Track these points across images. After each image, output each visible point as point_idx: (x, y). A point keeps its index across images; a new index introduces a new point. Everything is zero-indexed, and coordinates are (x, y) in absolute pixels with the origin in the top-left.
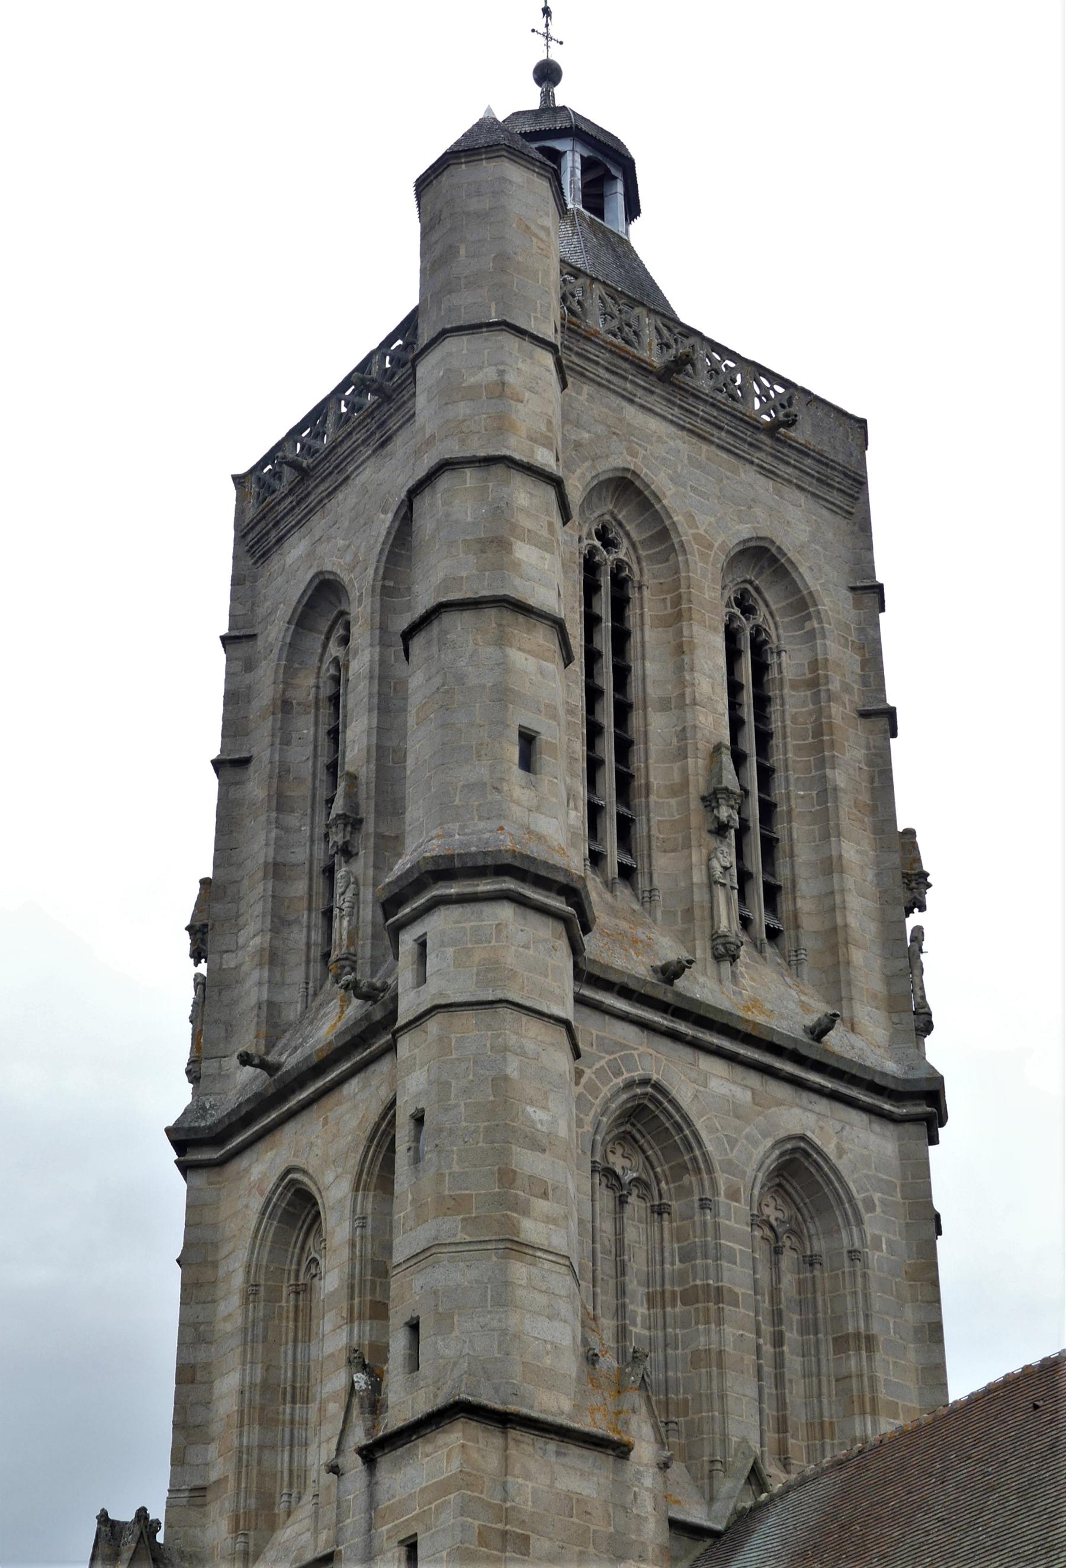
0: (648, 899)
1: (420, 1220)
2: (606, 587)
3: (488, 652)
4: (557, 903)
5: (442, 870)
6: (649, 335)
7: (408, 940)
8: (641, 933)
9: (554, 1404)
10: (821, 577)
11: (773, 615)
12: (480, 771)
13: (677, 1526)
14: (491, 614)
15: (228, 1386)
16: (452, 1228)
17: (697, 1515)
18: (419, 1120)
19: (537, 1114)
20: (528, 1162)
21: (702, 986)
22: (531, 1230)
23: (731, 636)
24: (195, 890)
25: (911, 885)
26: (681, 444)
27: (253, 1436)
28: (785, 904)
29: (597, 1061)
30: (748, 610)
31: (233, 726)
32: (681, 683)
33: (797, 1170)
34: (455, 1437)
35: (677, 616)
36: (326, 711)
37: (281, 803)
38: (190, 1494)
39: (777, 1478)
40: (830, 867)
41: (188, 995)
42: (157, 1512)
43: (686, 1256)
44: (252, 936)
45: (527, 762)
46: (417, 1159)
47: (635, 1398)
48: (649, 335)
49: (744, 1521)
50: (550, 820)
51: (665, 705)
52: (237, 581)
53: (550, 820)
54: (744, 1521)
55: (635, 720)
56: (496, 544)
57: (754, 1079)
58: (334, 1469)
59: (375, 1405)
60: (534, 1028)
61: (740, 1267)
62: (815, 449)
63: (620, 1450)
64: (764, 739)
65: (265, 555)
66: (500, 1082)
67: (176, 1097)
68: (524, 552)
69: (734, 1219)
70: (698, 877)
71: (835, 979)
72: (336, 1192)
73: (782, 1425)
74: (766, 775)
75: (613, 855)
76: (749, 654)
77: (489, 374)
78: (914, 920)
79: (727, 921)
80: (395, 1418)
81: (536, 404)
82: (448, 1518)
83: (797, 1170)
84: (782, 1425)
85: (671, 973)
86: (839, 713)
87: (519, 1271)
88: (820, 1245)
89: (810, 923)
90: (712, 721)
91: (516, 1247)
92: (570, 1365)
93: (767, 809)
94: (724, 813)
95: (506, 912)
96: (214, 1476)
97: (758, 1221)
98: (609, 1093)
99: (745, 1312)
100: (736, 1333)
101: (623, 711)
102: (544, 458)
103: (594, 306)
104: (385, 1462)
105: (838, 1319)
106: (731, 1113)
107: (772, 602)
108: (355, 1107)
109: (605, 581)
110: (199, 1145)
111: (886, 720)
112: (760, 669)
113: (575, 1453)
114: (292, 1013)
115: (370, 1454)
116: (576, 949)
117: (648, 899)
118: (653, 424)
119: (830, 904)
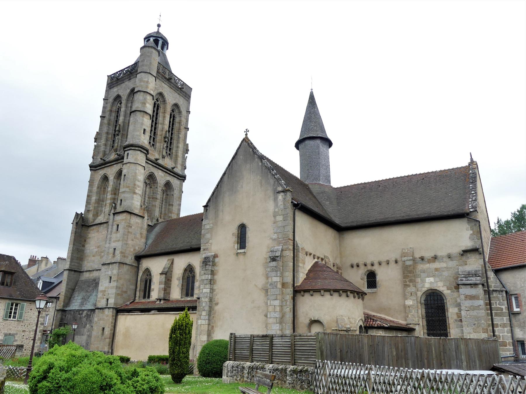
0: (155, 149)
1: (124, 188)
2: (156, 107)
3: (141, 118)
4: (145, 152)
5: (132, 145)
6: (167, 73)
7: (126, 153)
8: (154, 153)
9: (137, 212)
10: (183, 110)
11: (176, 113)
12: (138, 133)
13: (149, 225)
14: (142, 113)
15: (94, 198)
16: (127, 190)
17: (150, 224)
18: (125, 175)
19: (139, 177)
20: (137, 183)
21: (160, 162)
22: (137, 191)
23: (171, 115)
24: (96, 133)
25: (187, 151)
26: (169, 89)
27: (96, 205)
28: (171, 151)
29: (147, 169)
30: (173, 112)
31: (104, 112)
32: (164, 121)
33: (168, 185)
34: (125, 214)
35: (164, 112)
36: (116, 113)
37: (109, 124)
38: (87, 211)
39: (160, 220)
40: (178, 147)
41: (93, 147)
42: (83, 213)
43: (153, 193)
44: (103, 141)
45: (144, 133)
46: (124, 180)
47: (146, 212)
48: (167, 73)
49: (155, 225)
50: (144, 140)
51: (161, 124)
52: (106, 91)
53: (144, 140)
54: (155, 225)
55: (157, 125)
56: (144, 104)
57: (164, 173)
58: (109, 215)
59: (115, 208)
60: (140, 167)
61: (159, 196)
62: (184, 91)
63: (143, 217)
64: (172, 129)
65: (111, 88)
66: (136, 173)
67: (90, 161)
68: (147, 105)
69: (160, 190)
70: (162, 147)
71: (176, 162)
72: (111, 178)
73: (161, 213)
74: (172, 134)
75: (152, 143)
76: (172, 117)
77: (146, 80)
78: (186, 155)
79: (164, 153)
80: (118, 211)
81: (152, 85)
82: (123, 223)
83: (168, 185)
84: (161, 213)
85: (157, 160)
86: (182, 127)
87: (135, 196)
88: (169, 193)
89: (174, 154)
90: (166, 127)
91: (135, 193)
92: (139, 207)
93: (171, 138)
94: (166, 140)
95: (139, 152)
96: (91, 209)
97: (162, 190)
98: (147, 173)
99: (159, 201)
100: (158, 203)
101: (156, 123)
102: (152, 92)
103: (161, 69)
104: (116, 215)
105: (169, 202)
106: (161, 177)
107: (176, 111)
108: (115, 168)
109: (156, 106)
110: (93, 167)
111: (189, 112)
112: (173, 120)
113: (138, 218)
114: (107, 152)
115: (114, 214)
116: (146, 156)
117: (155, 149)
118: (166, 86)
119: (177, 152)
